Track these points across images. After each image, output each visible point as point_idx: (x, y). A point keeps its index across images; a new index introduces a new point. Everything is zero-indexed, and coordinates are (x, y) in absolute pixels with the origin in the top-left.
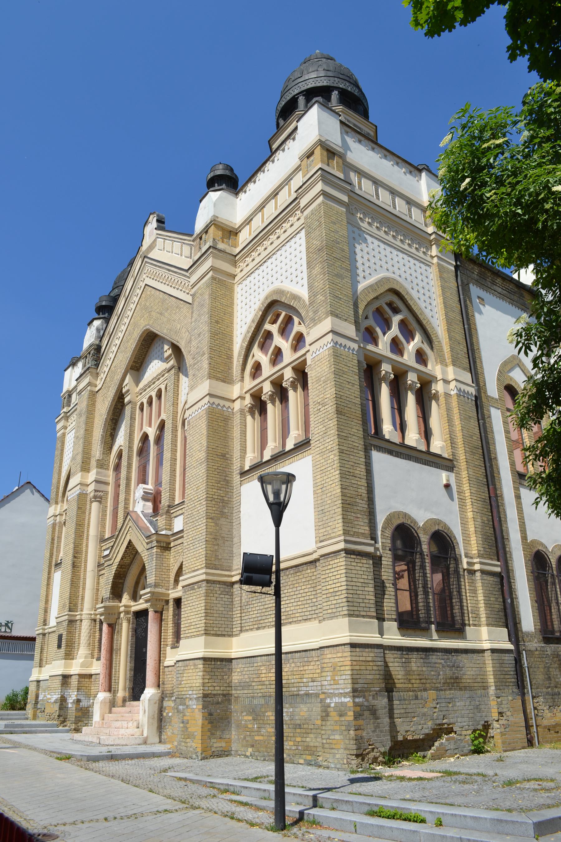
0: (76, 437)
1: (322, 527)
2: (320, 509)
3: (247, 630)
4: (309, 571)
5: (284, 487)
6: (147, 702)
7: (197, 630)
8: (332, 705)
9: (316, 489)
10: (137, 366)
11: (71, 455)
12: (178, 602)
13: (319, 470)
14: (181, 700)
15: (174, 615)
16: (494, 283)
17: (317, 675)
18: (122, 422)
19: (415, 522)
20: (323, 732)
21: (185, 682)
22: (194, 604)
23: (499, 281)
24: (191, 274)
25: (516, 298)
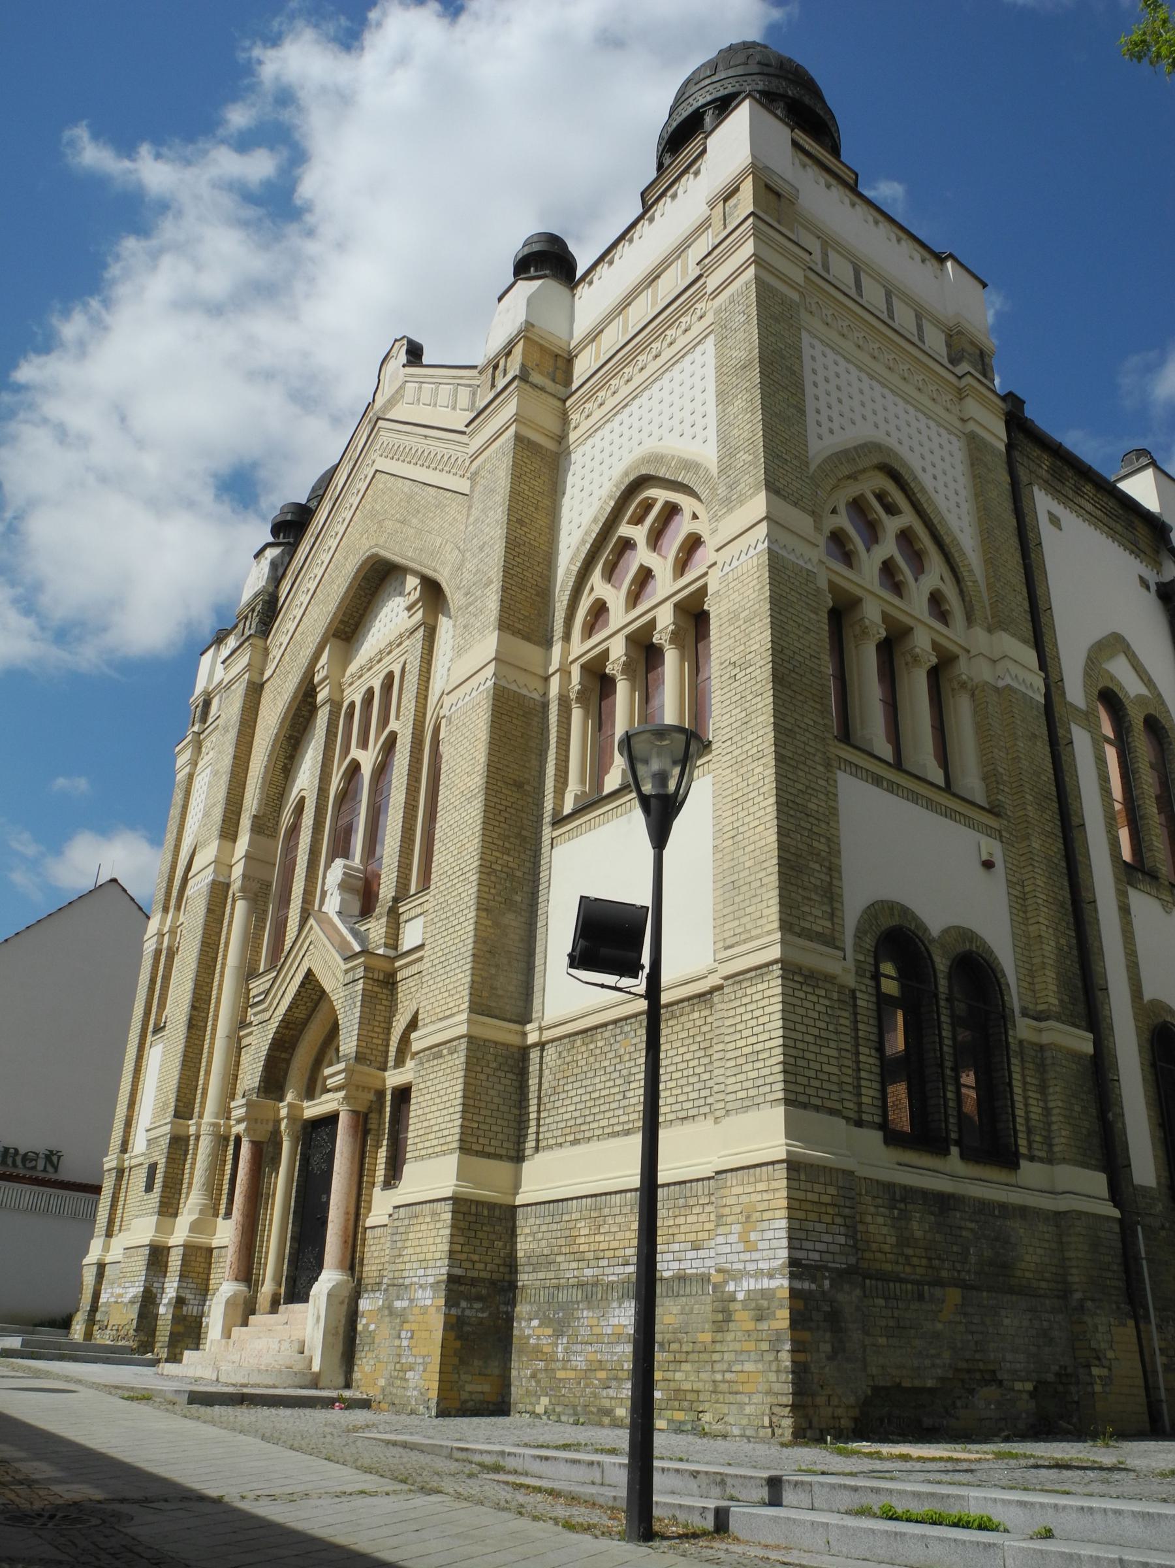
3: (550, 1147)
4: (696, 1015)
5: (676, 771)
6: (324, 1299)
7: (442, 1141)
8: (740, 1296)
10: (349, 627)
12: (403, 1095)
16: (1078, 491)
17: (705, 1235)
18: (309, 743)
19: (926, 929)
20: (716, 1357)
21: (410, 1251)
23: (1088, 488)
24: (473, 432)
25: (1119, 528)
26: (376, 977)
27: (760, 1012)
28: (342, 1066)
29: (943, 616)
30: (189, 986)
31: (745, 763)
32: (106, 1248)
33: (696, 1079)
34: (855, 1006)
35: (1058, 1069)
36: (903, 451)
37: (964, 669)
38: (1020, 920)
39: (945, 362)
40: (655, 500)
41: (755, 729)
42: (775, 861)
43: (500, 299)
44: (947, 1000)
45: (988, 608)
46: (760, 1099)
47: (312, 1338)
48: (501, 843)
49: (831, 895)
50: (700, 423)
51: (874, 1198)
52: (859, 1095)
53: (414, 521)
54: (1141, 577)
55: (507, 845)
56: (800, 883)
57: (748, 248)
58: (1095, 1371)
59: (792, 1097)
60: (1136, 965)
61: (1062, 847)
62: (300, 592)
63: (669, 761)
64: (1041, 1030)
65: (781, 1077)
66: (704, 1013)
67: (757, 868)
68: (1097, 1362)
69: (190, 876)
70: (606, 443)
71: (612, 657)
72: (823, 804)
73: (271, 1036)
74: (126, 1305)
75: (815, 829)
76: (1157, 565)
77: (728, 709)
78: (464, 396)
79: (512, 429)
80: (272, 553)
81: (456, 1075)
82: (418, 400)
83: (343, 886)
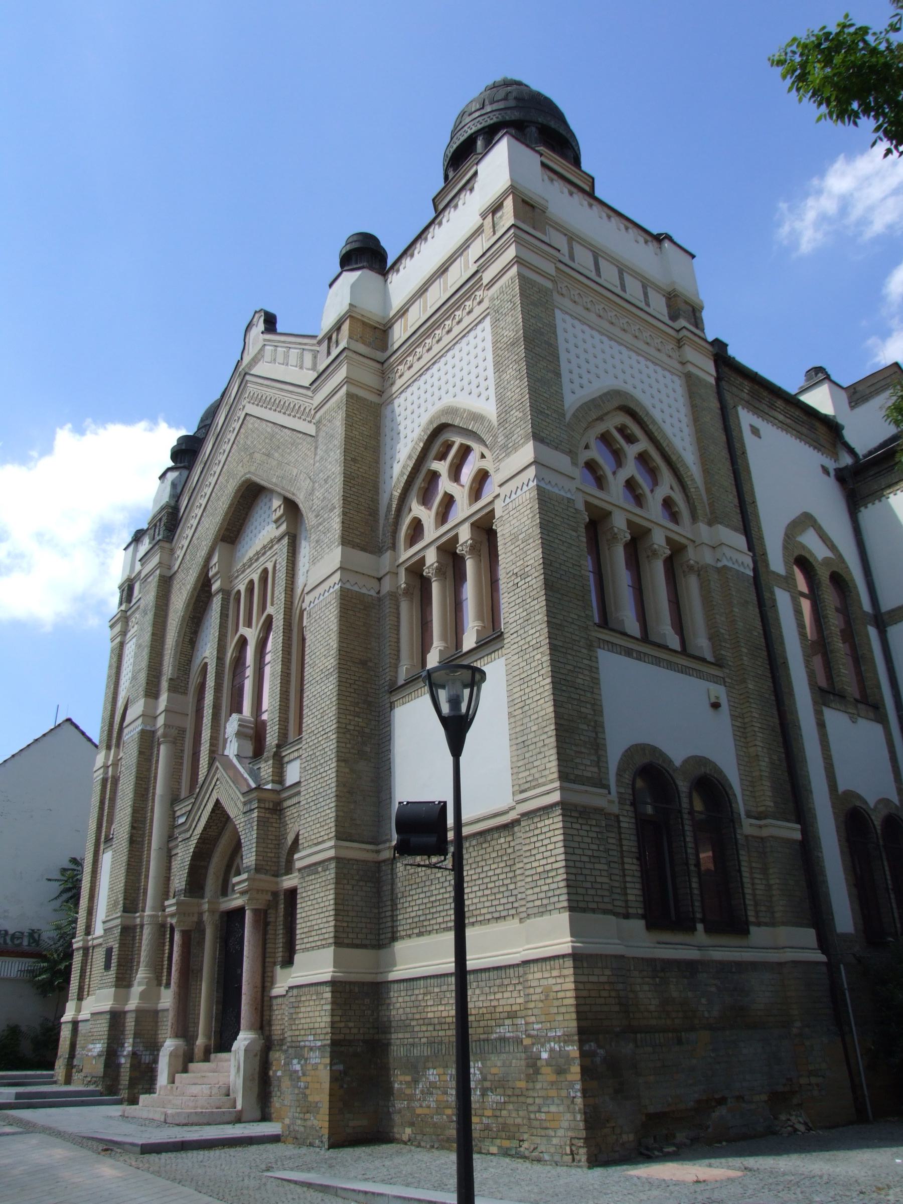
0: (139, 646)
1: (523, 768)
2: (520, 740)
4: (502, 840)
5: (467, 692)
6: (242, 1053)
7: (321, 937)
8: (545, 1055)
9: (512, 709)
10: (232, 531)
11: (130, 675)
12: (292, 893)
13: (518, 678)
14: (299, 1051)
15: (285, 916)
16: (772, 406)
19: (670, 762)
20: (530, 1101)
22: (317, 896)
23: (779, 403)
24: (314, 392)
25: (804, 431)
27: (547, 841)
28: (244, 876)
29: (674, 517)
30: (129, 811)
31: (528, 651)
32: (79, 1010)
33: (504, 889)
34: (619, 827)
36: (638, 394)
37: (691, 555)
38: (742, 744)
39: (666, 319)
40: (454, 442)
41: (534, 625)
42: (553, 727)
43: (331, 285)
44: (689, 813)
45: (707, 507)
46: (552, 907)
47: (235, 1084)
49: (597, 746)
50: (483, 385)
52: (626, 894)
53: (276, 455)
54: (823, 467)
55: (357, 709)
59: (575, 905)
61: (771, 685)
62: (199, 496)
63: (459, 685)
64: (760, 827)
65: (565, 890)
66: (508, 839)
67: (540, 732)
69: (125, 724)
70: (415, 397)
71: (428, 563)
72: (588, 678)
73: (192, 850)
74: (95, 1057)
75: (582, 698)
76: (835, 456)
77: (514, 609)
78: (308, 358)
79: (344, 390)
80: (171, 476)
81: (329, 887)
82: (275, 360)
83: (239, 734)
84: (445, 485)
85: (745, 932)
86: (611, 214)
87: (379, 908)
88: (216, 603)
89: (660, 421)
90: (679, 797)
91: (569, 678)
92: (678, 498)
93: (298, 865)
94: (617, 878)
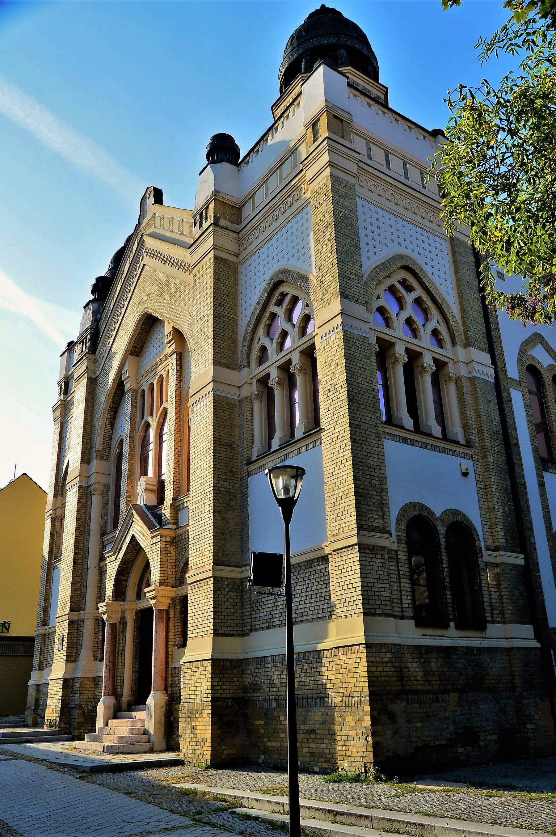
4: (321, 567)
13: (330, 460)
19: (433, 513)
21: (193, 685)
22: (201, 602)
26: (167, 540)
29: (440, 343)
30: (72, 542)
34: (398, 559)
35: (506, 575)
37: (451, 369)
43: (200, 174)
45: (463, 335)
48: (223, 477)
49: (383, 506)
51: (411, 654)
52: (402, 603)
55: (226, 477)
56: (366, 503)
57: (326, 158)
58: (529, 726)
60: (549, 513)
65: (361, 602)
68: (529, 722)
73: (116, 569)
81: (209, 596)
84: (281, 323)
85: (483, 628)
86: (399, 118)
87: (242, 609)
88: (128, 399)
89: (430, 275)
90: (439, 538)
91: (364, 461)
92: (443, 329)
93: (188, 581)
94: (396, 592)
